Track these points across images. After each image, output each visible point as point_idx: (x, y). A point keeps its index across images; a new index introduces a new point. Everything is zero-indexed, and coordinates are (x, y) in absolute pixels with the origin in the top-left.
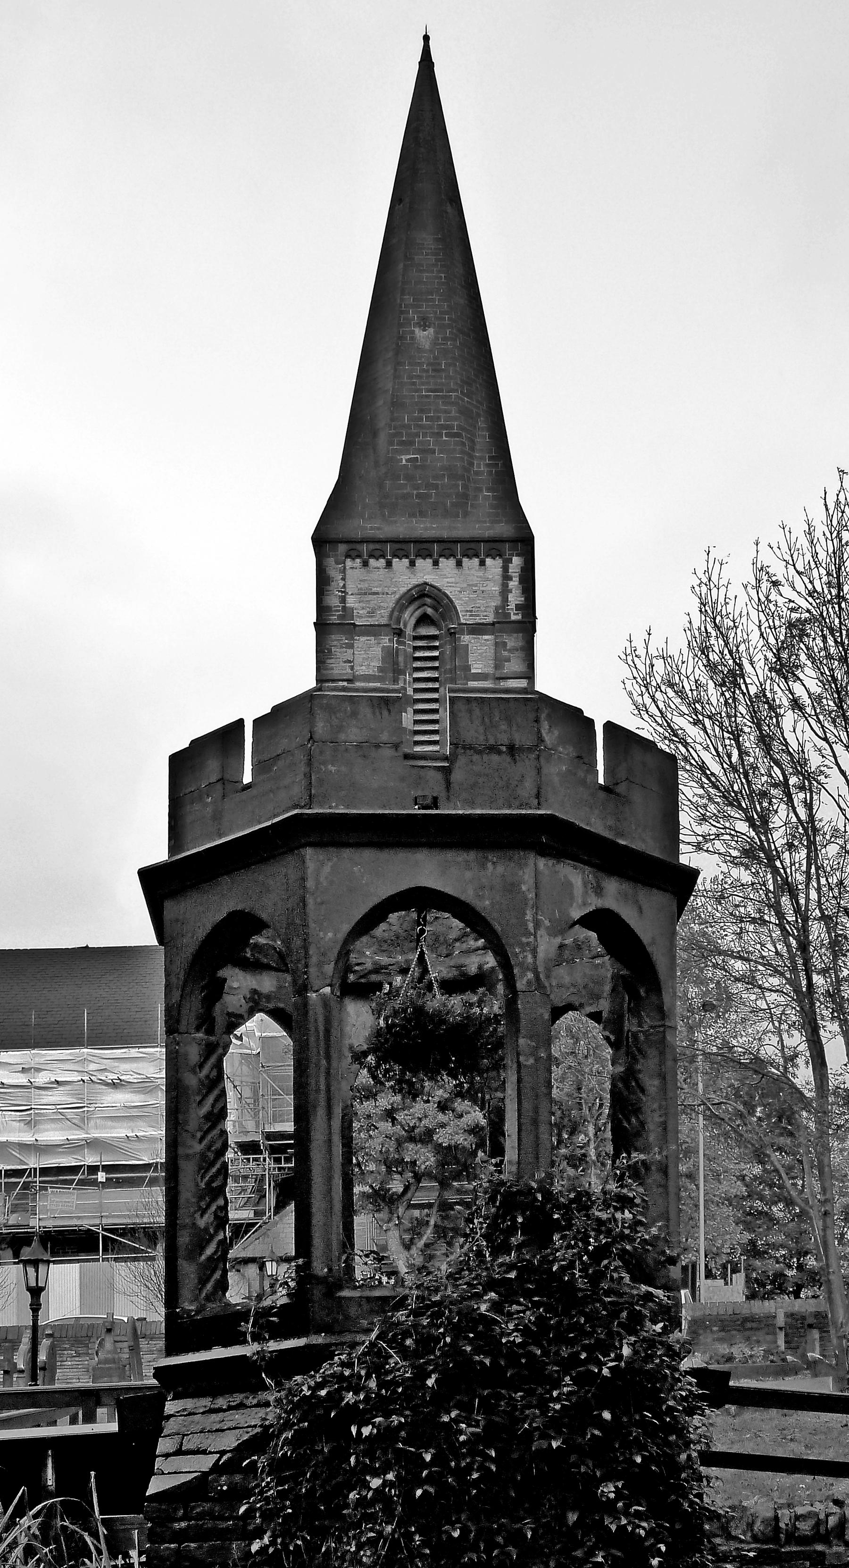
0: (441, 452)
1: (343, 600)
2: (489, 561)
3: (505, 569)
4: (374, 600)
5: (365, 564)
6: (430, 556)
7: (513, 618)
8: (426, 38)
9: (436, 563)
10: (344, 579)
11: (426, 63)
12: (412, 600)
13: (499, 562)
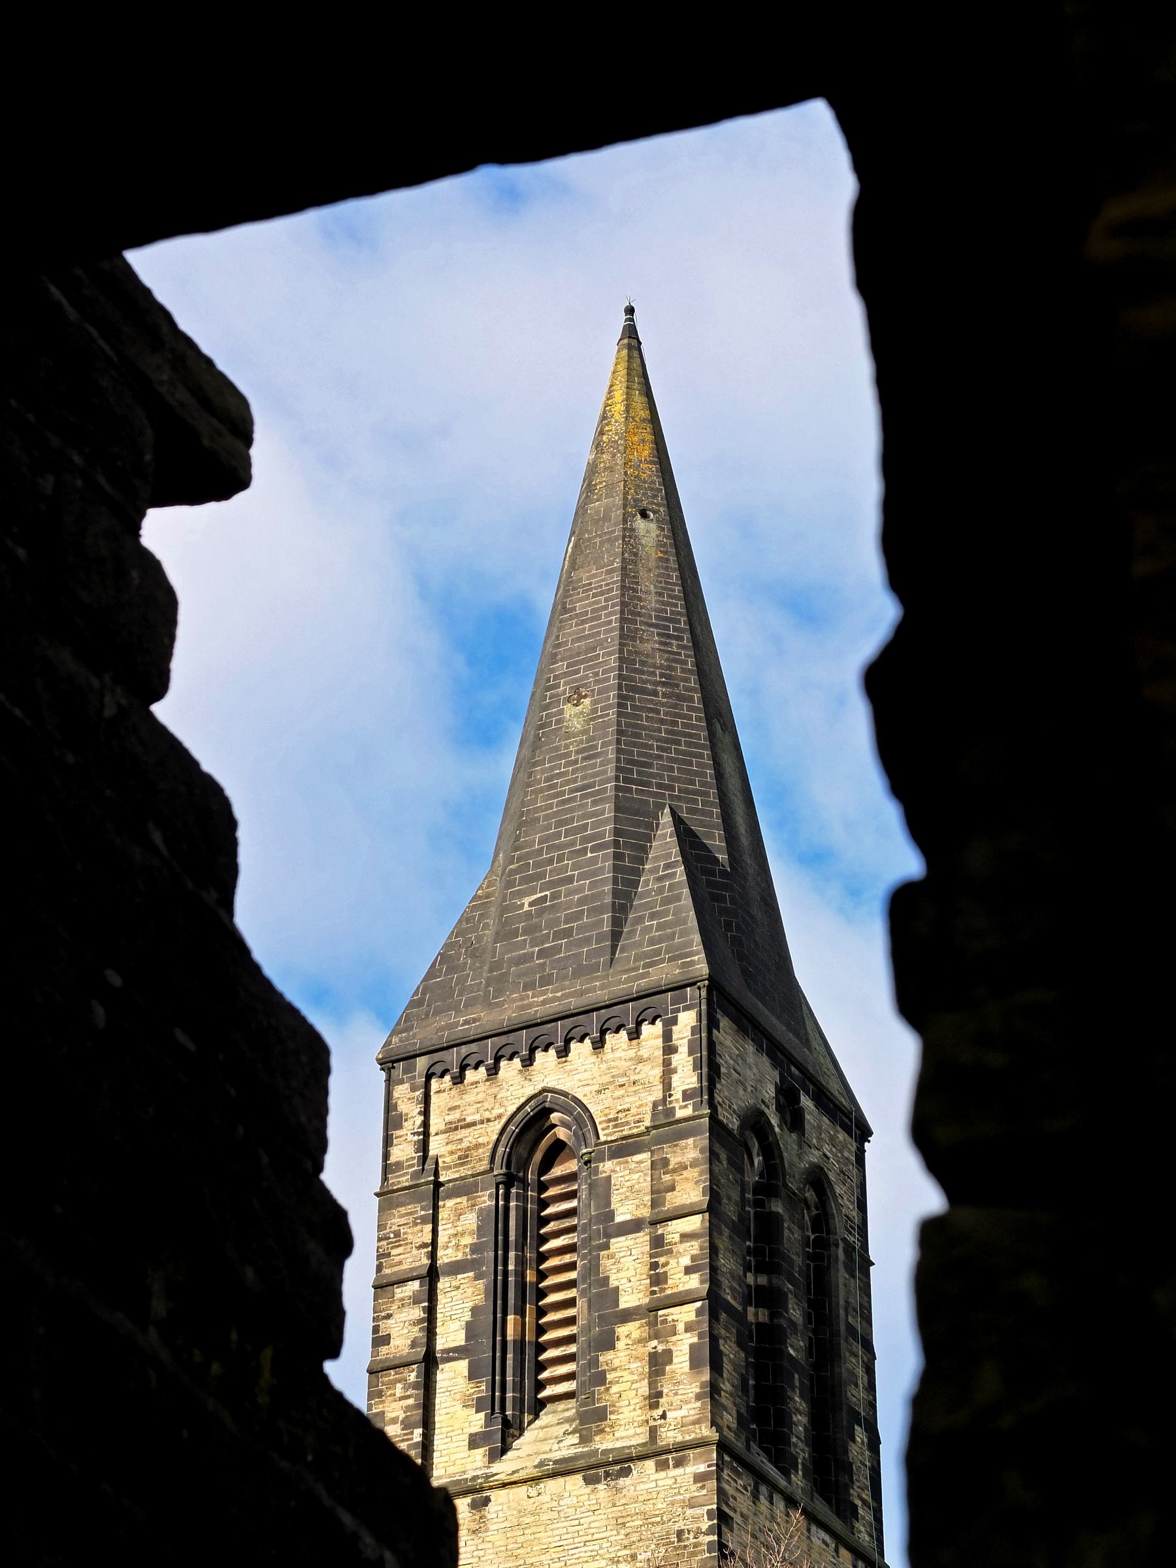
2: (646, 1029)
3: (667, 1036)
4: (468, 1137)
7: (680, 1114)
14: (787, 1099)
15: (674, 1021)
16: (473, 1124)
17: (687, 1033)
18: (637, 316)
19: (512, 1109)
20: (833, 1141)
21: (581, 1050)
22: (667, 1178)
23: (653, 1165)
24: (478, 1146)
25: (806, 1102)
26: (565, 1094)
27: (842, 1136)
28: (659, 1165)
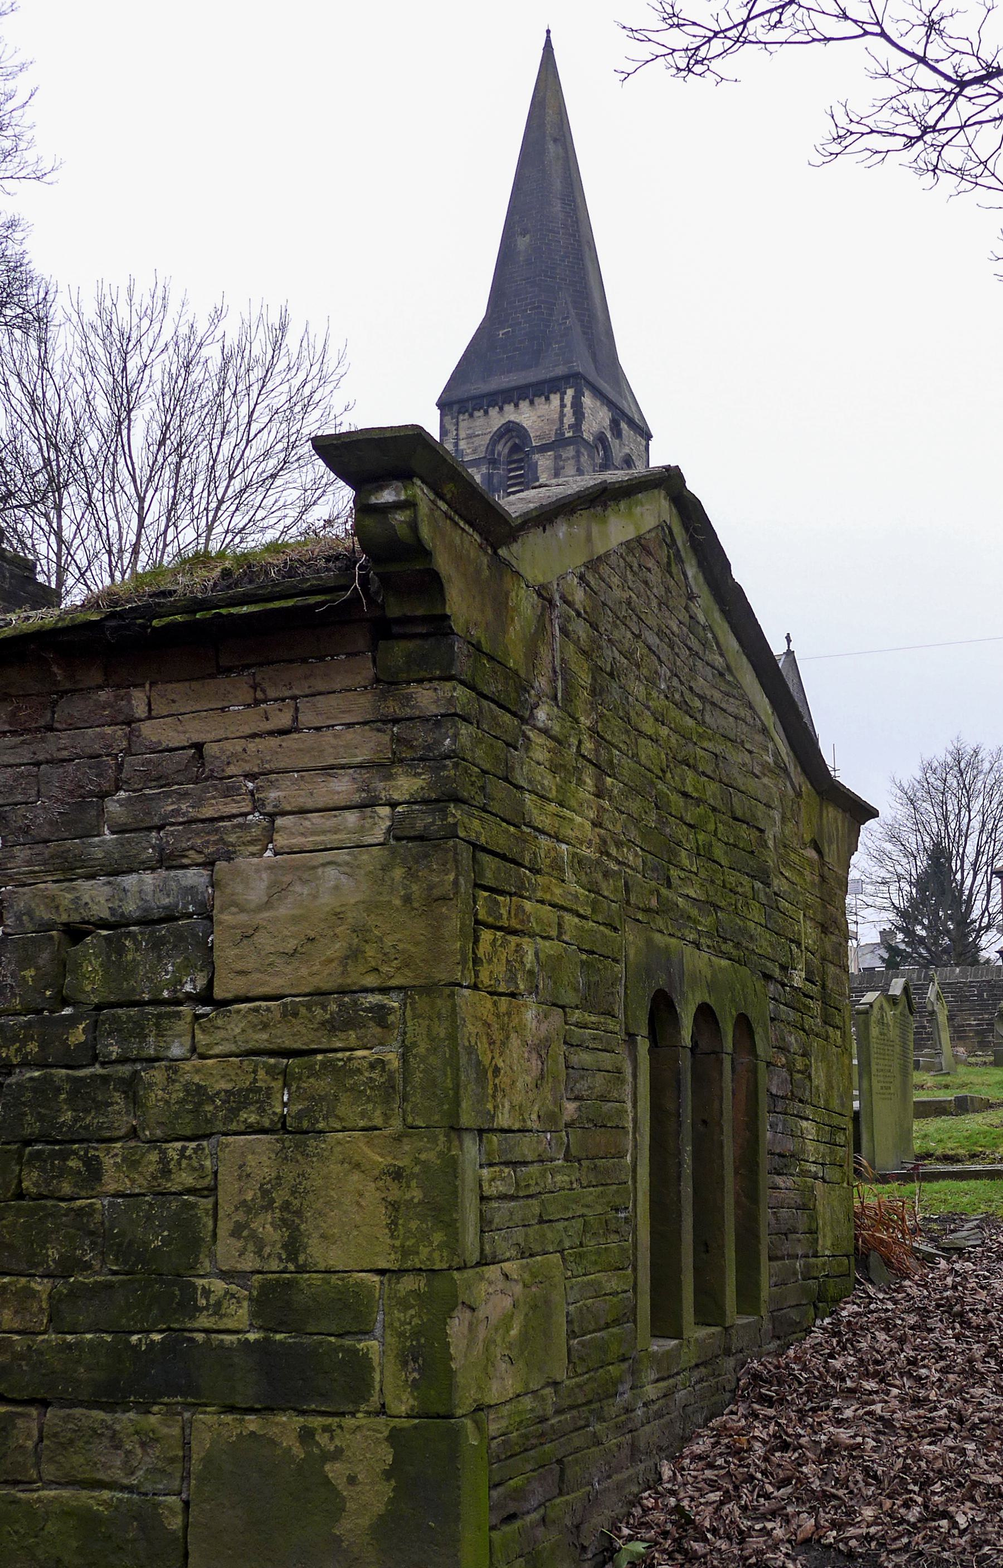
0: (525, 322)
1: (456, 445)
2: (552, 396)
3: (562, 399)
4: (477, 441)
5: (471, 416)
6: (496, 404)
7: (567, 435)
8: (548, 32)
9: (516, 405)
10: (457, 430)
11: (548, 48)
12: (501, 437)
13: (558, 396)
14: (615, 425)
15: (565, 393)
16: (478, 435)
17: (570, 399)
18: (551, 35)
19: (495, 429)
20: (635, 441)
21: (524, 405)
22: (561, 463)
23: (556, 458)
24: (480, 446)
25: (624, 426)
26: (518, 424)
27: (639, 439)
28: (558, 457)
